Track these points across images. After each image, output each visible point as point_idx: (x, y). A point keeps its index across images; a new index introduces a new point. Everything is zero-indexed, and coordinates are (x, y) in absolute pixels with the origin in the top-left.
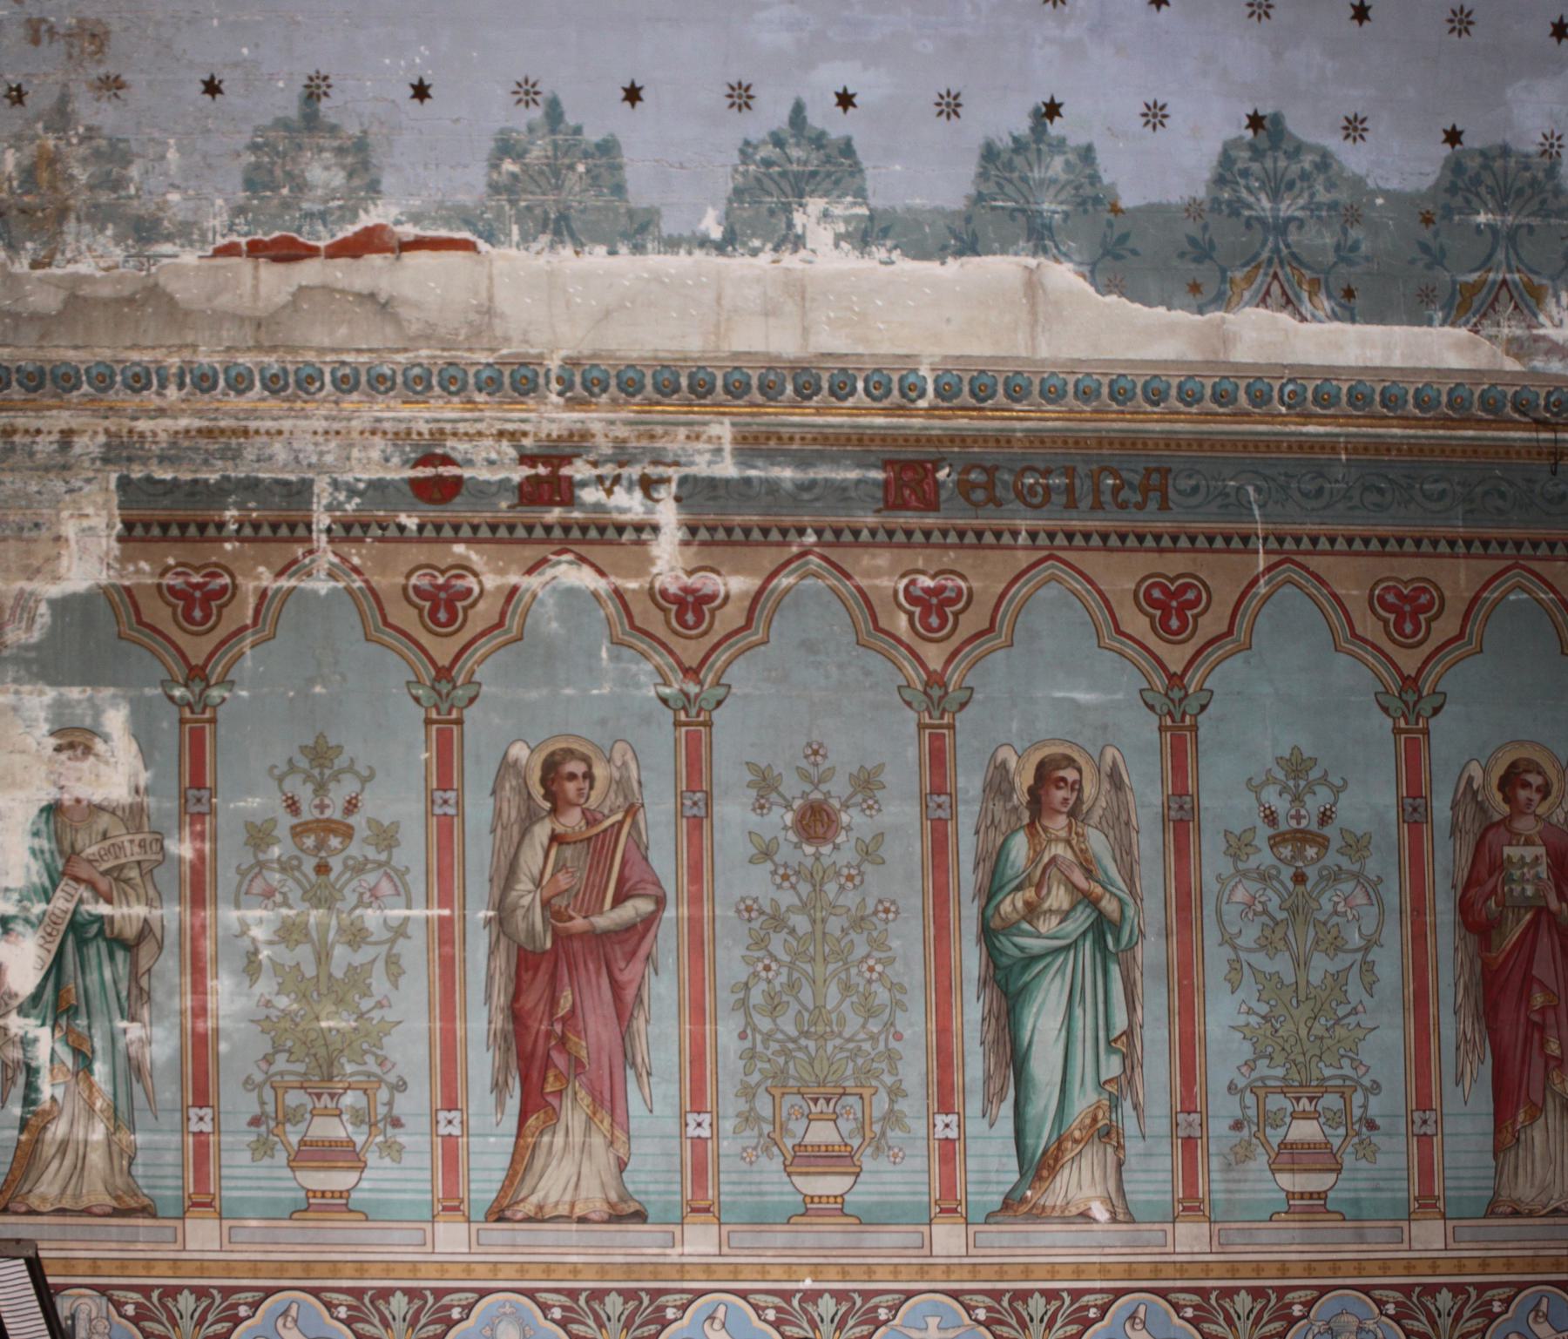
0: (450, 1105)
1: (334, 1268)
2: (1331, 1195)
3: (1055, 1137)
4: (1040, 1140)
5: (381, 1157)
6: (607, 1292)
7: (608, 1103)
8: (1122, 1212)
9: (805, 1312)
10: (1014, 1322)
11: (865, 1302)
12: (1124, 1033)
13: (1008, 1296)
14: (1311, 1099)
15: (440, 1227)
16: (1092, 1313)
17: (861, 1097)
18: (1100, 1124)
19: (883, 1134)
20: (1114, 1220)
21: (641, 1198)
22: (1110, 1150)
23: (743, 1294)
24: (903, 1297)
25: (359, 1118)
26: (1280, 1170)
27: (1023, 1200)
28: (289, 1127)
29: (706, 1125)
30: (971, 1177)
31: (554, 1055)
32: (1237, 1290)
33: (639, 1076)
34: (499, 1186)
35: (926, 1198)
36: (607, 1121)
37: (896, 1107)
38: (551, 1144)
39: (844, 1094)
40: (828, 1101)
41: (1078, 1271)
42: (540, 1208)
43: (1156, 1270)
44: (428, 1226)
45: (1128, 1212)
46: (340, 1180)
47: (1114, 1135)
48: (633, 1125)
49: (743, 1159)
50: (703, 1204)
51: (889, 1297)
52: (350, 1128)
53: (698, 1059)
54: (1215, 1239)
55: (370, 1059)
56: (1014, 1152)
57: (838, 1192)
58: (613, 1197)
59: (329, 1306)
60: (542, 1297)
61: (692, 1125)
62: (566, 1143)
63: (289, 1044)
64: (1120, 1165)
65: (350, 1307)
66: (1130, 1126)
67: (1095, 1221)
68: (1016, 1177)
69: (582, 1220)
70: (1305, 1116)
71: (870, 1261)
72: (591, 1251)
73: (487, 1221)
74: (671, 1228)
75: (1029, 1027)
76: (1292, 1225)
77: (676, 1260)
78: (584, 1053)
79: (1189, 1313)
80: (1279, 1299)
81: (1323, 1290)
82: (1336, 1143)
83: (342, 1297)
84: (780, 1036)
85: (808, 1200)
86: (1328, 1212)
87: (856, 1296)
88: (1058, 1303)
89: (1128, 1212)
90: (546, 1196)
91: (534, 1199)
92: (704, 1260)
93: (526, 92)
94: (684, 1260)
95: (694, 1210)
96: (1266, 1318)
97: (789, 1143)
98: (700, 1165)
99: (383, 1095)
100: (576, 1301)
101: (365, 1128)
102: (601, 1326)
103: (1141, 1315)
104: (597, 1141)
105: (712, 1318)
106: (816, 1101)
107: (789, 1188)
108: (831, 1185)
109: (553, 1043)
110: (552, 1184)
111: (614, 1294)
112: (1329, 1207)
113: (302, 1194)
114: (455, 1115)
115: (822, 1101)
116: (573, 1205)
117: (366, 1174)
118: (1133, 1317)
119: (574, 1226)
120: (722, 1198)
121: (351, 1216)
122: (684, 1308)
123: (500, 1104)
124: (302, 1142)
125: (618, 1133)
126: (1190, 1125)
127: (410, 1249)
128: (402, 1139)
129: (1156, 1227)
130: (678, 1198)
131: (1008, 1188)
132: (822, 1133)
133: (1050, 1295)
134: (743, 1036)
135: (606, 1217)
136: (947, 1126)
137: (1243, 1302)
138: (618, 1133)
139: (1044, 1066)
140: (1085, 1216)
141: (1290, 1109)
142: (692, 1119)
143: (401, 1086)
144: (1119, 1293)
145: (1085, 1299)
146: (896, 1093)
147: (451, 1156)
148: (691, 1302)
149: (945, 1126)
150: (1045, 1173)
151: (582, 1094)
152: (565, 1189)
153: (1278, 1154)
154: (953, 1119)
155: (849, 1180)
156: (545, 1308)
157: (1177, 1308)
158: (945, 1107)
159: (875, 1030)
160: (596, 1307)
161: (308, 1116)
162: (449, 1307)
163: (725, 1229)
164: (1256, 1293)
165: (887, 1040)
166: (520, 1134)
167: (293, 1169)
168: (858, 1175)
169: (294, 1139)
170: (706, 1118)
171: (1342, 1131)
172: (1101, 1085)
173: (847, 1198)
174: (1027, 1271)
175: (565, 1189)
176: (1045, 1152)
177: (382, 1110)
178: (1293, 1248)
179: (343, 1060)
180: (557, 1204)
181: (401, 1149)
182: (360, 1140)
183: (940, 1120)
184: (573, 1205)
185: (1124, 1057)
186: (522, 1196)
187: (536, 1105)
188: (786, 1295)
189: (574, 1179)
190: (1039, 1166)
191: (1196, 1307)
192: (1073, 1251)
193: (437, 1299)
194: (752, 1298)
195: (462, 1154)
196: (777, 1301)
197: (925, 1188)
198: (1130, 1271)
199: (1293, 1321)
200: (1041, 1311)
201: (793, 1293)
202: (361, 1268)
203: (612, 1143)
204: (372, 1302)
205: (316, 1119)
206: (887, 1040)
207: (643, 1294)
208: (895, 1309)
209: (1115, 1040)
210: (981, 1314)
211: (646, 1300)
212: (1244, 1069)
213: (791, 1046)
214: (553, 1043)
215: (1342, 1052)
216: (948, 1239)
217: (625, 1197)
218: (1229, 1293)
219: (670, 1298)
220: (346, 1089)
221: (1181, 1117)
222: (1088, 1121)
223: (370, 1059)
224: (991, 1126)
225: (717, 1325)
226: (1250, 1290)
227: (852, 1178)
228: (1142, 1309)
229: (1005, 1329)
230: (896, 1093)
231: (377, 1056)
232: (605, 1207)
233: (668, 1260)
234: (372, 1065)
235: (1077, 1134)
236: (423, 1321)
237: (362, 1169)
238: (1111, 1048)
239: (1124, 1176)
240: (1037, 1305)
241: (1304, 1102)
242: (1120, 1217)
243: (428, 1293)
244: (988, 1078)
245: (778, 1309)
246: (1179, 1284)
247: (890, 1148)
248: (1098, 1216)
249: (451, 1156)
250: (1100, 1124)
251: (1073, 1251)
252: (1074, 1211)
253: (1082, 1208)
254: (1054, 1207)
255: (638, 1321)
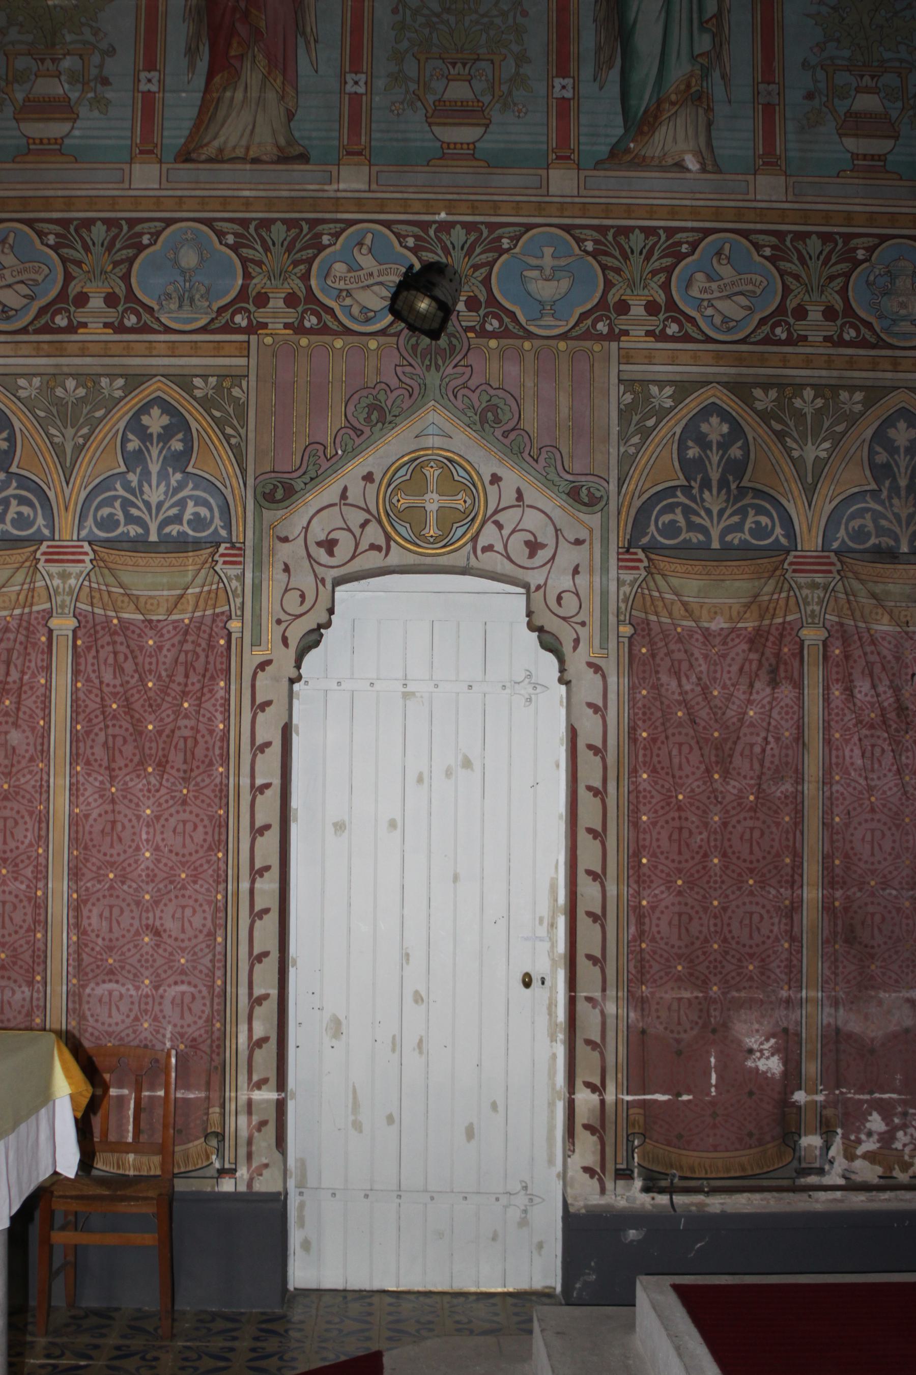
0: (151, 65)
1: (47, 203)
2: (889, 157)
3: (654, 100)
4: (643, 101)
5: (91, 110)
6: (274, 221)
7: (282, 66)
8: (711, 163)
9: (440, 240)
10: (617, 254)
11: (491, 232)
12: (715, 16)
13: (612, 231)
14: (873, 77)
15: (136, 167)
16: (684, 248)
17: (493, 63)
18: (693, 90)
19: (510, 93)
20: (704, 170)
21: (306, 142)
22: (701, 111)
23: (387, 224)
24: (523, 229)
25: (75, 78)
26: (846, 135)
27: (627, 151)
28: (16, 86)
29: (362, 83)
30: (583, 130)
31: (238, 25)
32: (808, 234)
33: (307, 43)
34: (187, 133)
35: (545, 147)
36: (280, 79)
37: (521, 71)
38: (232, 98)
39: (478, 59)
40: (464, 65)
41: (673, 212)
42: (221, 150)
43: (739, 214)
44: (126, 167)
45: (716, 164)
46: (56, 129)
47: (704, 100)
48: (302, 83)
49: (392, 111)
50: (356, 148)
51: (511, 229)
52: (66, 86)
53: (357, 30)
54: (790, 190)
55: (87, 31)
56: (619, 109)
57: (471, 140)
58: (282, 142)
59: (41, 234)
60: (219, 225)
61: (350, 83)
62: (245, 97)
63: (21, 19)
64: (709, 124)
65: (57, 235)
66: (718, 92)
67: (688, 170)
68: (621, 131)
69: (256, 161)
70: (868, 90)
71: (496, 198)
72: (261, 187)
73: (176, 162)
74: (329, 168)
75: (634, 9)
76: (856, 181)
77: (332, 194)
78: (263, 24)
79: (768, 252)
80: (845, 243)
81: (884, 238)
82: (894, 114)
83: (51, 227)
84: (426, 11)
85: (445, 146)
86: (887, 172)
87: (483, 227)
88: (655, 239)
89: (716, 164)
90: (225, 143)
91: (216, 143)
92: (357, 195)
93: (269, 703)
94: (340, 195)
95: (349, 153)
96: (833, 260)
97: (431, 98)
98: (356, 113)
99: (96, 59)
100: (247, 229)
101: (79, 86)
102: (267, 249)
103: (727, 252)
104: (271, 96)
105: (360, 244)
106: (454, 65)
107: (431, 136)
108: (466, 134)
109: (238, 16)
110: (231, 133)
111: (279, 223)
112: (477, 156)
113: (24, 141)
114: (154, 75)
115: (459, 65)
116: (248, 149)
117: (78, 124)
118: (719, 253)
119: (248, 167)
120: (373, 143)
121: (475, 163)
122: (337, 235)
123: (192, 66)
124: (27, 99)
125: (289, 89)
126: (769, 93)
127: (111, 186)
128: (109, 95)
129: (740, 177)
130: (336, 143)
131: (614, 140)
132: (458, 91)
133: (649, 232)
134: (395, 11)
135: (275, 158)
136: (564, 87)
137: (814, 245)
138: (289, 89)
139: (647, 40)
140: (680, 166)
141: (855, 85)
142: (350, 78)
143: (111, 51)
144: (708, 232)
145: (679, 236)
146: (522, 59)
147: (149, 107)
148: (343, 230)
149: (562, 87)
150: (646, 129)
151: (260, 57)
152: (242, 136)
153: (844, 121)
154: (568, 82)
155: (481, 130)
156: (220, 235)
157: (757, 247)
158: (563, 72)
159: (505, 8)
160: (264, 234)
161: (33, 77)
162: (141, 234)
163: (375, 169)
164: (826, 238)
165: (515, 18)
166: (207, 89)
167: (17, 120)
168: (487, 126)
169: (20, 96)
170: (362, 77)
171: (899, 104)
172: (693, 58)
173: (477, 145)
174: (629, 211)
175: (242, 136)
176: (645, 112)
177: (94, 72)
178: (857, 201)
179: (65, 31)
180: (234, 148)
181: (108, 102)
182: (74, 96)
183: (558, 82)
184: (248, 149)
185: (714, 36)
186: (205, 141)
187: (222, 68)
188: (424, 226)
189: (250, 127)
190: (640, 123)
191: (773, 247)
192: (669, 195)
193: (131, 228)
194: (396, 228)
195: (158, 106)
196: (416, 230)
197: (544, 139)
198: (717, 214)
199: (857, 263)
200: (283, 236)
201: (429, 224)
202: (69, 202)
203: (283, 98)
204: (76, 231)
205: (40, 80)
206: (515, 18)
207: (303, 224)
208: (516, 239)
209: (707, 22)
210: (590, 246)
211: (306, 228)
212: (815, 50)
213: (435, 19)
214: (238, 16)
215: (899, 39)
216: (562, 182)
217: (292, 141)
218: (802, 236)
219: (325, 226)
220: (64, 55)
221: (762, 87)
222: (682, 87)
223: (87, 31)
224: (601, 88)
225: (364, 251)
226: (821, 235)
227: (482, 129)
228: (727, 246)
229: (609, 259)
230: (522, 59)
231: (91, 27)
232: (275, 151)
233: (325, 195)
234: (88, 35)
235: (673, 97)
236: (118, 246)
237: (75, 121)
238: (702, 28)
239: (714, 134)
240: (637, 240)
241: (867, 79)
242: (709, 168)
243: (123, 222)
244: (599, 49)
245: (417, 237)
246: (759, 227)
247: (515, 104)
248: (690, 166)
249: (149, 107)
250: (693, 90)
251: (669, 195)
252: (670, 161)
253: (677, 159)
254: (653, 158)
255: (298, 246)
